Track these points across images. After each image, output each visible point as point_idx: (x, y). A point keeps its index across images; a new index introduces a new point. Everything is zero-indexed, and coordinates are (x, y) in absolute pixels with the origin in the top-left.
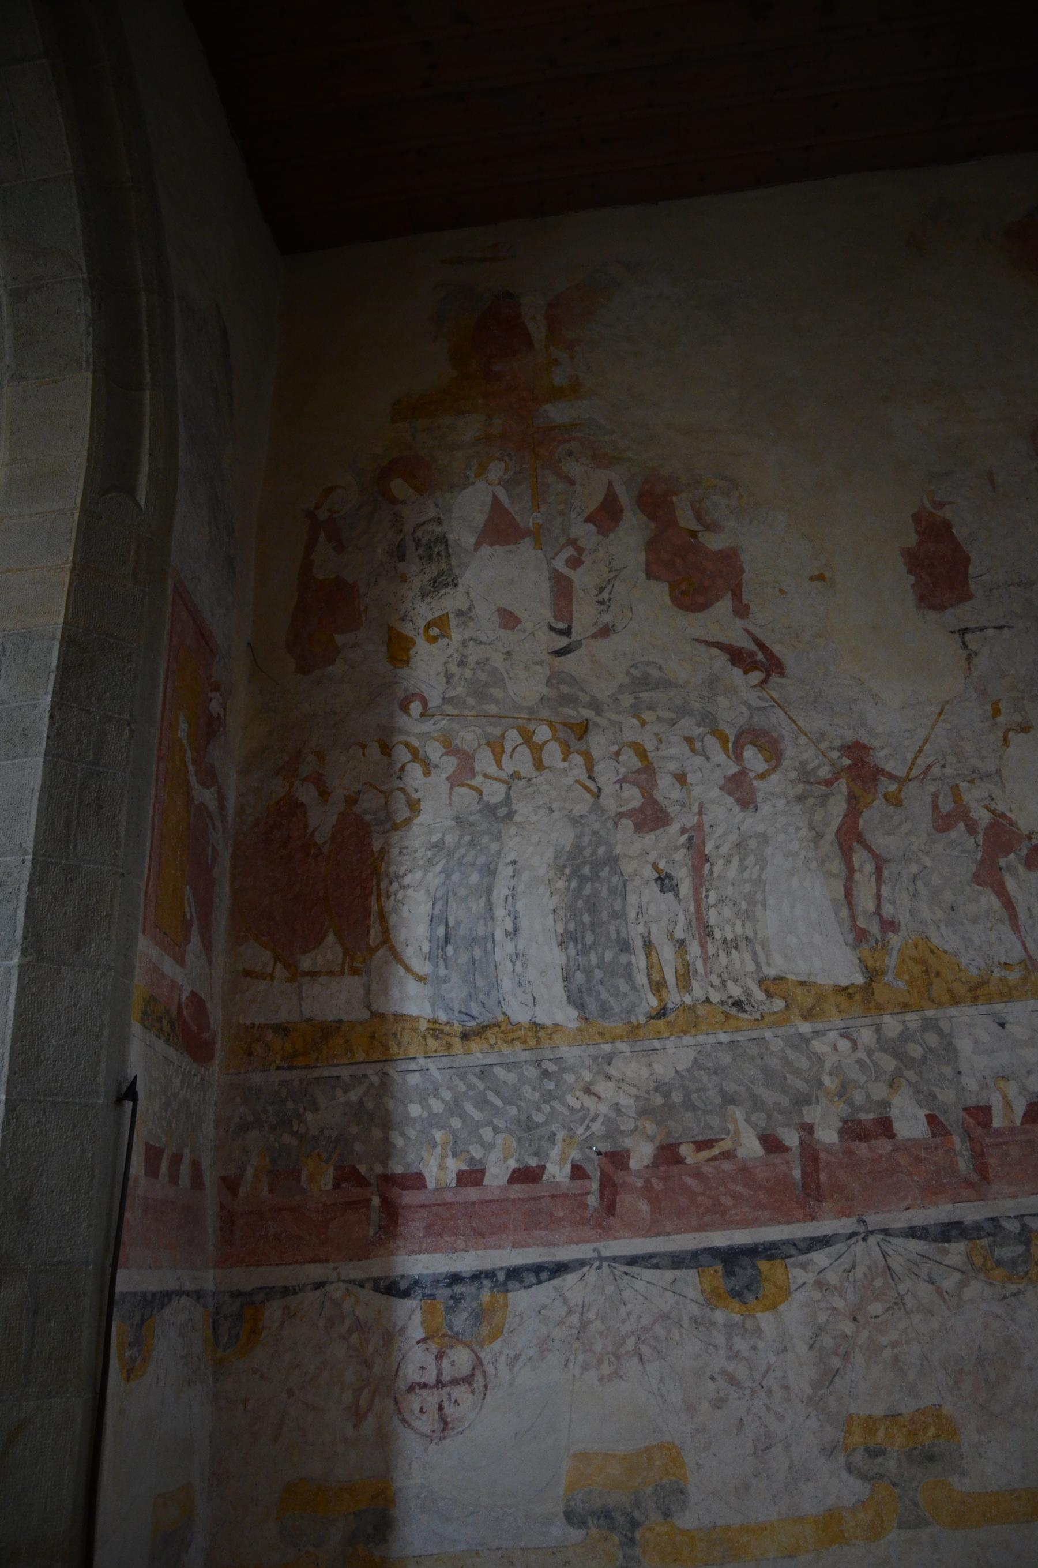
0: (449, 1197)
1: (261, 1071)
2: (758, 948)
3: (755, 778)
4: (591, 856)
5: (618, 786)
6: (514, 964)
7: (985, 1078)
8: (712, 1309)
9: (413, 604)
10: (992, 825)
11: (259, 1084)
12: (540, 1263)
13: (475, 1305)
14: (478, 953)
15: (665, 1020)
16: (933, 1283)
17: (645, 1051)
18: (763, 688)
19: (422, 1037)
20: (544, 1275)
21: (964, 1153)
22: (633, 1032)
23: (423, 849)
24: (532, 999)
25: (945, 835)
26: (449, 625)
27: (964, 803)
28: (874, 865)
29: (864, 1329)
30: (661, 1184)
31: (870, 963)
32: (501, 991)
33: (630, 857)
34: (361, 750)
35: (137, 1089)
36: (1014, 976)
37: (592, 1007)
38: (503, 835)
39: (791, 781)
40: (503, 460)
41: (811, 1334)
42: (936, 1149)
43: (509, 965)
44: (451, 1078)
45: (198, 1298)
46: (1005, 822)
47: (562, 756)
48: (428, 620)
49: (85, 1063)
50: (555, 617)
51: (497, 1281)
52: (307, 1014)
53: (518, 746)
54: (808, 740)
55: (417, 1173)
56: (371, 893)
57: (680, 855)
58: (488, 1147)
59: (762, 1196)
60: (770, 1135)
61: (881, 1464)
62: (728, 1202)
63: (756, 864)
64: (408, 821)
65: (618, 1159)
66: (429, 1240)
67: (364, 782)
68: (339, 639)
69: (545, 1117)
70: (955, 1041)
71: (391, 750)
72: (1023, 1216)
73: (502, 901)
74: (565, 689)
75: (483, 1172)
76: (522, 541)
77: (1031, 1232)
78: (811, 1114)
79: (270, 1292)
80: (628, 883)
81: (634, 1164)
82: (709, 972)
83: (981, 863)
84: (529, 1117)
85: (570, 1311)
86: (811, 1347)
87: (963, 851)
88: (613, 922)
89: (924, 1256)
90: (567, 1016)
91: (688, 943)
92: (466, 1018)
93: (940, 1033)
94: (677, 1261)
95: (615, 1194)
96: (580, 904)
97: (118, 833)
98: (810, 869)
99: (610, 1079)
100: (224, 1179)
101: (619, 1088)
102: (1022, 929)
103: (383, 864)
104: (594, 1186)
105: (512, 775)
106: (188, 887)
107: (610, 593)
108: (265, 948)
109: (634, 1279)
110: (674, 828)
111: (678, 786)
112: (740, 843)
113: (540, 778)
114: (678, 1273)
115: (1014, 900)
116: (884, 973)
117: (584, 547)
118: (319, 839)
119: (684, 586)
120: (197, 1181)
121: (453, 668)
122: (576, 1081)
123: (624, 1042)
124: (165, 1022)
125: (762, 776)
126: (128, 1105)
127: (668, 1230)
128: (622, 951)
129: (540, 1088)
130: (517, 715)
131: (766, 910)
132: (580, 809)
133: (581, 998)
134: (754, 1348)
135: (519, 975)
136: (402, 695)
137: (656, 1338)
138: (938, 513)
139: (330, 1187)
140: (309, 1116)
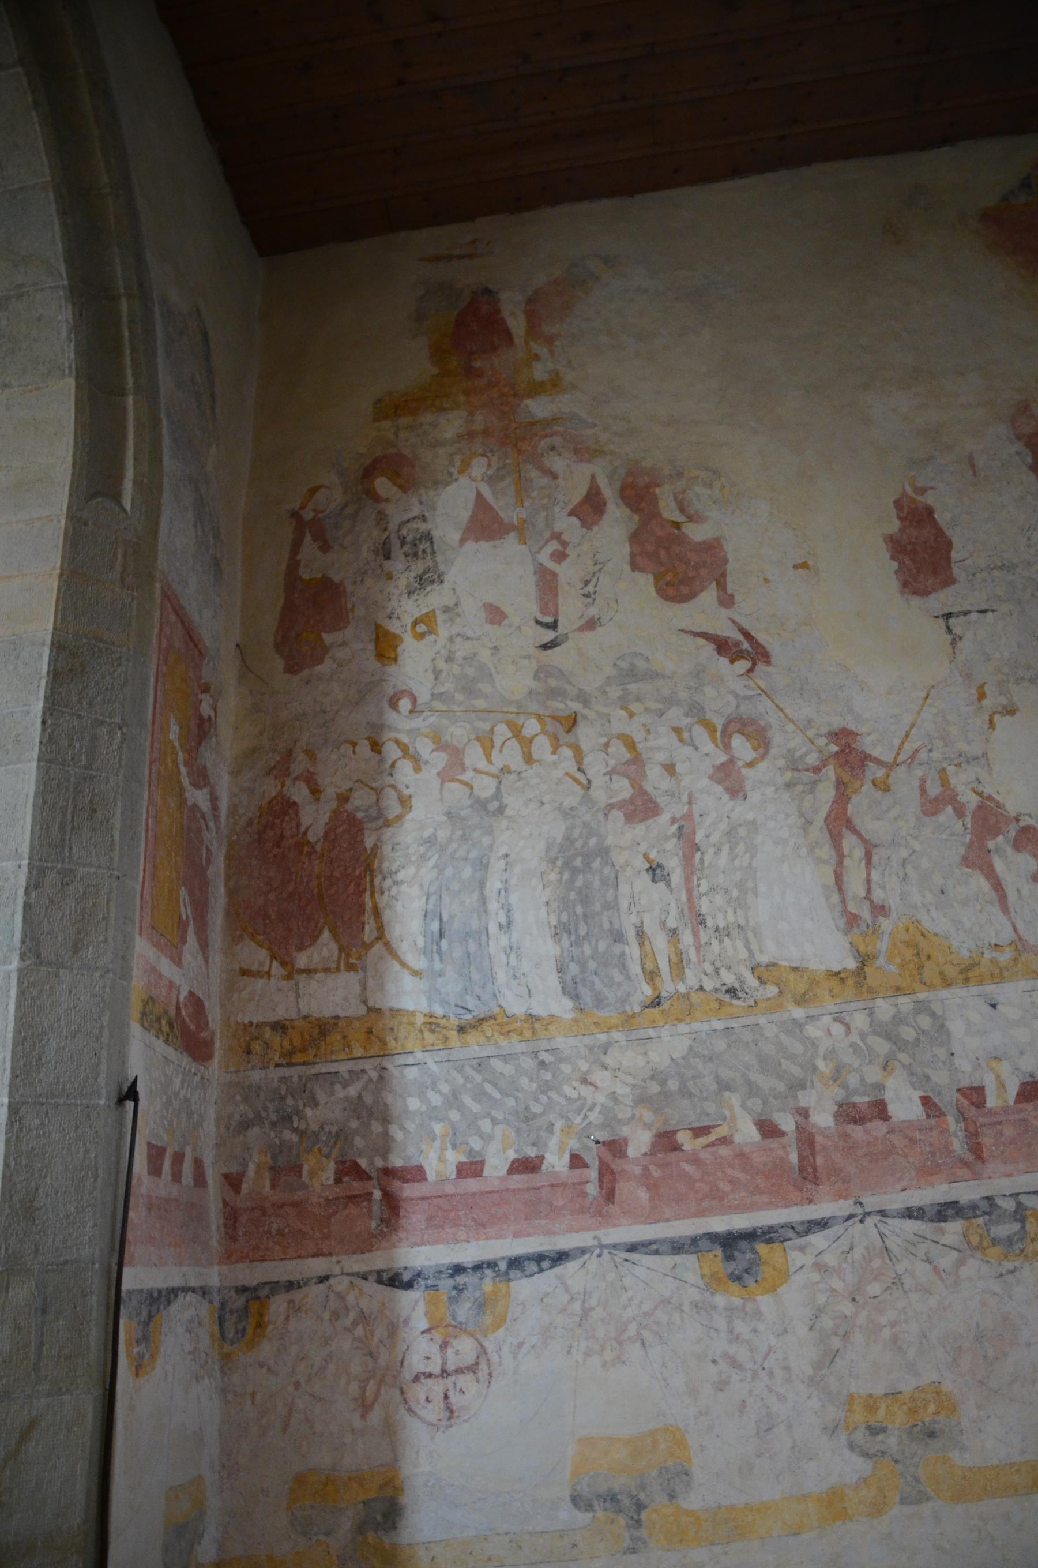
0: (449, 1189)
3: (743, 766)
5: (607, 778)
6: (508, 957)
10: (980, 808)
13: (477, 1294)
14: (472, 947)
16: (930, 1263)
20: (545, 1264)
22: (628, 1021)
23: (416, 845)
26: (436, 621)
29: (863, 1309)
30: (659, 1172)
31: (862, 949)
32: (496, 984)
36: (1005, 957)
37: (587, 997)
41: (810, 1316)
42: (931, 1130)
45: (204, 1293)
46: (992, 805)
47: (551, 749)
48: (414, 618)
51: (499, 1271)
52: (304, 1011)
53: (506, 741)
55: (417, 1166)
56: (365, 890)
57: (671, 844)
60: (765, 1121)
63: (746, 853)
64: (399, 818)
65: (615, 1147)
66: (430, 1232)
67: (355, 779)
68: (328, 638)
70: (948, 1024)
72: (1018, 1194)
74: (553, 683)
75: (482, 1163)
76: (506, 536)
78: (806, 1099)
79: (275, 1287)
81: (632, 1152)
82: (701, 961)
83: (970, 846)
84: (527, 1108)
87: (952, 835)
89: (920, 1236)
90: (563, 1007)
92: (462, 1011)
93: (933, 1015)
94: (677, 1247)
95: (614, 1181)
96: (573, 895)
97: (112, 836)
98: (799, 856)
99: (606, 1068)
100: (226, 1176)
102: (1011, 910)
104: (593, 1174)
106: (183, 888)
107: (595, 586)
108: (261, 946)
110: (664, 818)
111: (666, 774)
114: (678, 1259)
115: (1003, 883)
116: (875, 957)
118: (311, 837)
119: (669, 577)
120: (200, 1179)
121: (441, 664)
122: (573, 1071)
124: (164, 1022)
125: (750, 765)
126: (130, 1105)
127: (667, 1216)
128: (615, 941)
130: (505, 710)
133: (576, 988)
134: (755, 1331)
136: (390, 692)
137: (658, 1323)
138: (920, 498)
139: (331, 1181)
140: (309, 1112)
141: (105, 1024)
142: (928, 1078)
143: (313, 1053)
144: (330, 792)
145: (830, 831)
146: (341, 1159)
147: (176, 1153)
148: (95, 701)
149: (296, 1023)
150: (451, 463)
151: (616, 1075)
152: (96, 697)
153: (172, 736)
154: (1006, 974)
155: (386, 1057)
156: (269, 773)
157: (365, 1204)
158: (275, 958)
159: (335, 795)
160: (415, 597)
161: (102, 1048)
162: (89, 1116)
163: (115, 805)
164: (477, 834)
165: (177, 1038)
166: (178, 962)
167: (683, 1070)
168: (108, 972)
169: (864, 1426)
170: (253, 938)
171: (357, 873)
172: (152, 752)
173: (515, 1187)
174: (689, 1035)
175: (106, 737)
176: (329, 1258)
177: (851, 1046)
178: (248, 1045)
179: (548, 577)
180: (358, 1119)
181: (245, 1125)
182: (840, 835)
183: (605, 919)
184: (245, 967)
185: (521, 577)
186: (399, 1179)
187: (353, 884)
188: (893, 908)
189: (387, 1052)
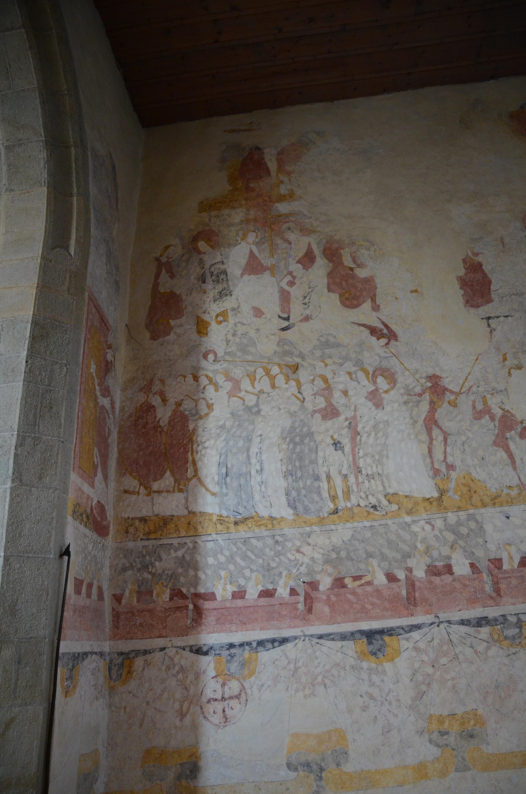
0: (228, 605)
2: (384, 478)
3: (383, 393)
5: (313, 397)
6: (261, 487)
7: (499, 544)
8: (361, 661)
10: (503, 416)
13: (241, 659)
14: (242, 481)
16: (473, 648)
20: (276, 644)
21: (489, 582)
22: (321, 521)
23: (215, 429)
25: (479, 421)
26: (228, 315)
27: (489, 405)
28: (443, 437)
29: (438, 671)
31: (441, 487)
34: (183, 379)
36: (514, 493)
37: (300, 508)
39: (401, 394)
40: (255, 232)
41: (411, 674)
42: (474, 580)
43: (258, 488)
44: (229, 545)
45: (101, 655)
46: (509, 415)
47: (285, 382)
50: (281, 311)
51: (252, 647)
54: (409, 374)
55: (211, 592)
56: (188, 451)
57: (345, 431)
60: (390, 573)
61: (447, 739)
63: (383, 436)
64: (207, 415)
65: (313, 585)
67: (185, 394)
68: (172, 322)
70: (484, 526)
72: (518, 614)
74: (287, 348)
75: (245, 592)
76: (265, 273)
77: (522, 622)
78: (411, 563)
79: (138, 653)
80: (318, 446)
81: (321, 588)
82: (359, 491)
83: (497, 436)
84: (268, 564)
86: (411, 680)
87: (488, 430)
88: (311, 466)
89: (468, 634)
90: (288, 513)
91: (348, 476)
92: (236, 514)
93: (477, 521)
94: (343, 637)
95: (312, 603)
97: (60, 421)
98: (410, 439)
99: (309, 545)
100: (114, 595)
102: (518, 469)
103: (195, 436)
104: (301, 599)
105: (260, 391)
106: (96, 448)
107: (309, 299)
108: (135, 478)
110: (342, 418)
114: (344, 643)
115: (514, 455)
116: (448, 491)
118: (161, 424)
119: (347, 295)
120: (101, 597)
121: (230, 337)
122: (293, 546)
124: (84, 516)
125: (386, 392)
126: (66, 558)
127: (339, 621)
128: (315, 480)
130: (262, 361)
131: (388, 459)
132: (294, 408)
133: (295, 504)
134: (382, 681)
135: (263, 492)
136: (204, 350)
137: (333, 676)
138: (476, 258)
139: (168, 599)
140: (157, 564)
141: (54, 516)
142: (473, 553)
143: (160, 534)
144: (172, 401)
145: (426, 427)
148: (53, 352)
150: (237, 235)
152: (54, 350)
153: (92, 371)
154: (514, 501)
156: (141, 390)
157: (185, 611)
158: (142, 485)
159: (174, 403)
160: (217, 302)
161: (52, 529)
164: (246, 424)
166: (92, 485)
167: (349, 547)
168: (56, 489)
169: (437, 731)
171: (185, 442)
172: (81, 378)
176: (165, 639)
177: (434, 536)
178: (127, 529)
179: (285, 294)
180: (182, 568)
181: (124, 569)
182: (431, 428)
184: (126, 489)
185: (272, 294)
186: (202, 599)
187: (182, 448)
188: (457, 466)
189: (198, 534)
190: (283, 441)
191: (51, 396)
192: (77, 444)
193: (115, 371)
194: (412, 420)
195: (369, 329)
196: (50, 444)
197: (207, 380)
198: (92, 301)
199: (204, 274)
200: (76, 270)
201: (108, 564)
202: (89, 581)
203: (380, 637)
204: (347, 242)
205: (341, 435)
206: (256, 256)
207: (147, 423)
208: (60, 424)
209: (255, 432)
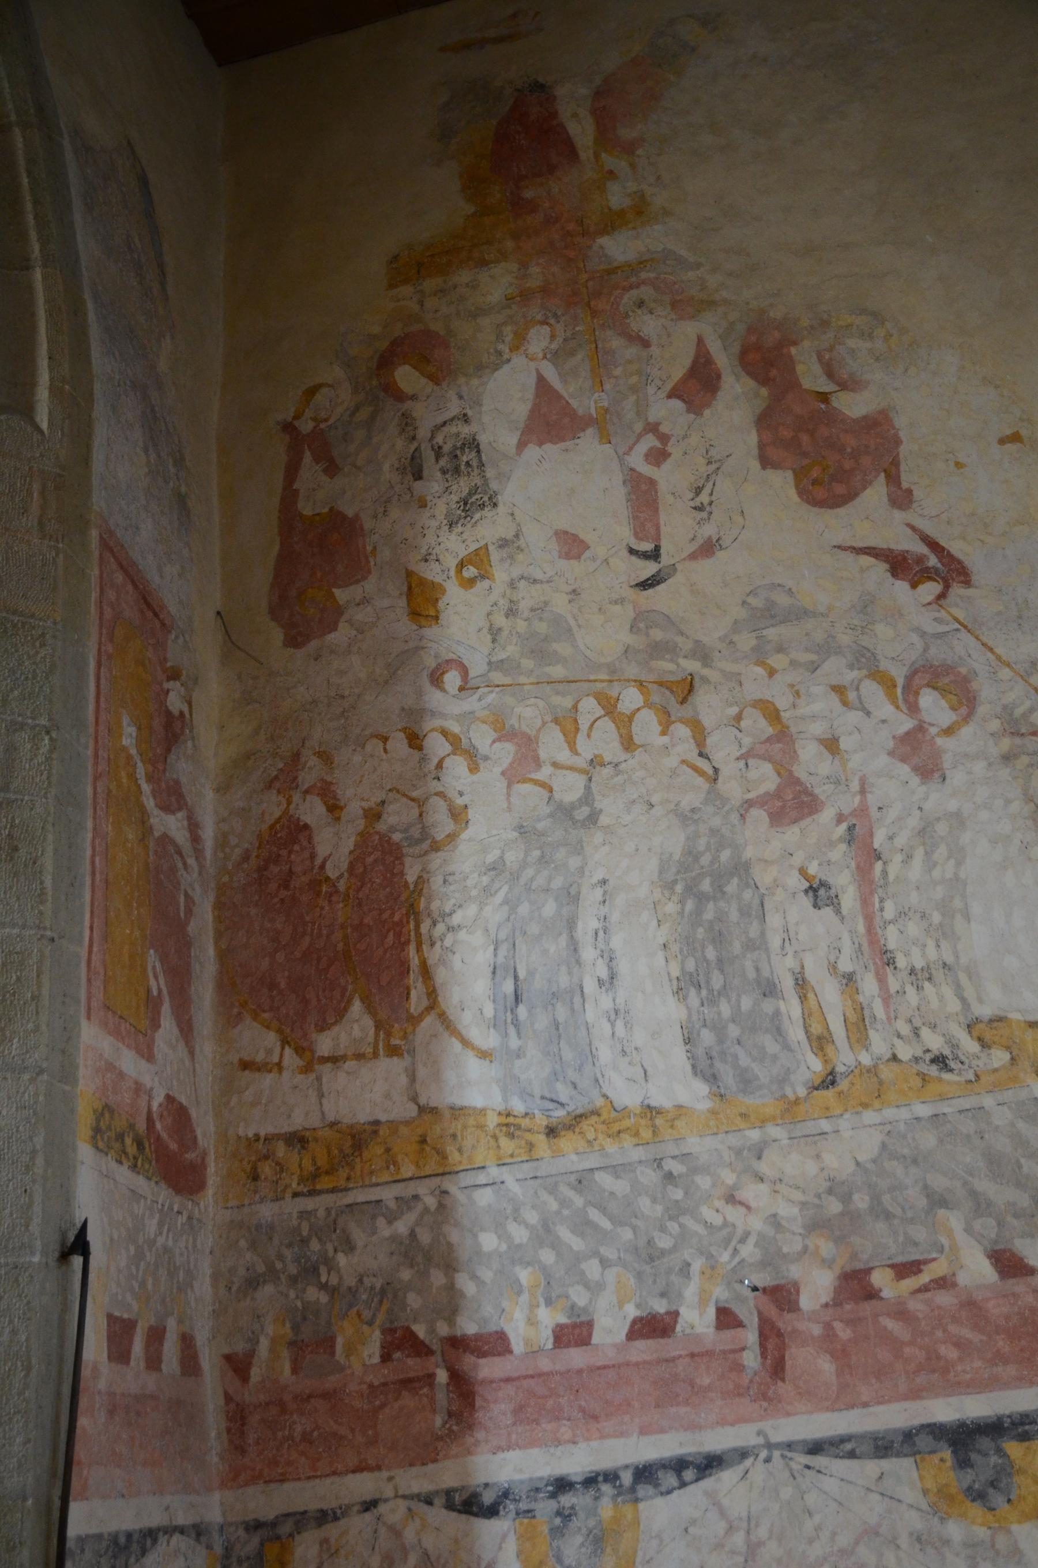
0: (545, 1364)
1: (272, 1201)
3: (938, 735)
4: (712, 863)
5: (742, 764)
6: (613, 1025)
9: (438, 537)
11: (269, 1219)
12: (681, 1456)
13: (591, 1523)
14: (562, 1013)
15: (832, 1090)
17: (810, 1136)
18: (941, 606)
19: (491, 1136)
20: (689, 1474)
23: (476, 875)
24: (643, 1072)
30: (849, 1331)
33: (766, 861)
34: (381, 744)
35: (88, 1239)
37: (729, 1079)
38: (585, 844)
40: (547, 324)
44: (536, 1193)
45: (199, 1534)
47: (660, 728)
48: (460, 558)
49: (11, 1206)
50: (636, 535)
51: (621, 1486)
52: (331, 1117)
53: (595, 721)
54: (1012, 674)
55: (497, 1332)
56: (408, 941)
58: (595, 1288)
59: (1001, 1343)
60: (1004, 1251)
62: (950, 1353)
63: (949, 858)
64: (452, 837)
66: (520, 1429)
67: (388, 788)
68: (341, 595)
69: (673, 1240)
71: (422, 741)
73: (589, 938)
74: (657, 634)
75: (590, 1325)
76: (581, 434)
79: (301, 1520)
80: (766, 898)
81: (806, 1302)
84: (650, 1242)
85: (731, 1527)
88: (749, 956)
91: (859, 977)
92: (551, 1106)
95: (782, 1348)
97: (42, 883)
98: (1030, 859)
100: (228, 1358)
101: (775, 1192)
103: (423, 899)
104: (751, 1337)
105: (592, 760)
106: (152, 951)
107: (711, 494)
108: (268, 1027)
109: (820, 1475)
110: (827, 815)
111: (826, 754)
112: (924, 829)
113: (631, 762)
117: (670, 433)
118: (331, 872)
119: (815, 473)
120: (190, 1364)
121: (500, 620)
122: (714, 1185)
123: (777, 1125)
124: (128, 1141)
125: (949, 731)
126: (77, 1261)
127: (864, 1398)
128: (765, 995)
129: (663, 1198)
130: (592, 677)
131: (969, 922)
132: (690, 800)
133: (712, 1065)
136: (431, 663)
139: (376, 1359)
140: (342, 1260)
141: (38, 1147)
143: (345, 1175)
144: (354, 809)
146: (388, 1325)
147: (151, 1329)
148: (11, 697)
149: (320, 1133)
150: (500, 337)
151: (776, 1188)
152: (12, 690)
153: (126, 742)
155: (447, 1176)
156: (269, 786)
157: (425, 1390)
158: (288, 1043)
159: (361, 812)
160: (459, 528)
161: (34, 1181)
162: (17, 1280)
163: (44, 840)
164: (561, 854)
165: (150, 1163)
166: (147, 1054)
168: (41, 1072)
170: (255, 1017)
171: (396, 918)
172: (96, 763)
173: (640, 1359)
174: (881, 1127)
175: (28, 746)
176: (377, 1474)
178: (255, 1169)
179: (644, 487)
180: (412, 1266)
181: (253, 1283)
183: (748, 964)
184: (247, 1058)
185: (605, 490)
186: (472, 1353)
187: (391, 933)
189: (448, 1169)
190: (667, 893)
191: (13, 817)
192: (95, 945)
193: (193, 739)
194: (1032, 805)
195: (887, 561)
196: (18, 949)
197: (447, 744)
198: (112, 551)
199: (417, 454)
200: (58, 470)
201: (208, 1272)
202: (153, 1321)
203: (993, 1444)
204: (805, 322)
205: (829, 863)
206: (556, 392)
207: (291, 872)
208: (43, 893)
209: (587, 873)
